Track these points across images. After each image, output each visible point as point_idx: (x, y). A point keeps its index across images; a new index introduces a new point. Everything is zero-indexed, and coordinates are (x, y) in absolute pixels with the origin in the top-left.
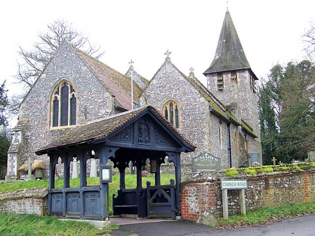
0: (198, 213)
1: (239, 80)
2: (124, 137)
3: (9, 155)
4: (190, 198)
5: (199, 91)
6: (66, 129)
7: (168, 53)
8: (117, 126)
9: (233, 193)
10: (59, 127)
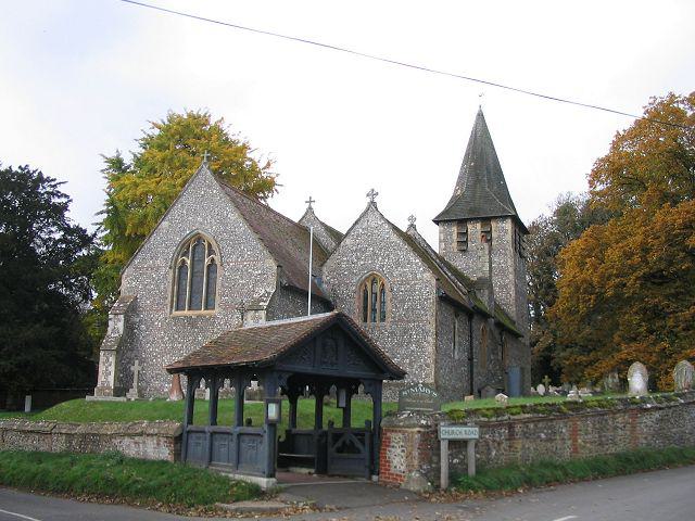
1: (494, 235)
3: (102, 353)
4: (393, 450)
7: (373, 194)
9: (458, 445)
10: (186, 312)
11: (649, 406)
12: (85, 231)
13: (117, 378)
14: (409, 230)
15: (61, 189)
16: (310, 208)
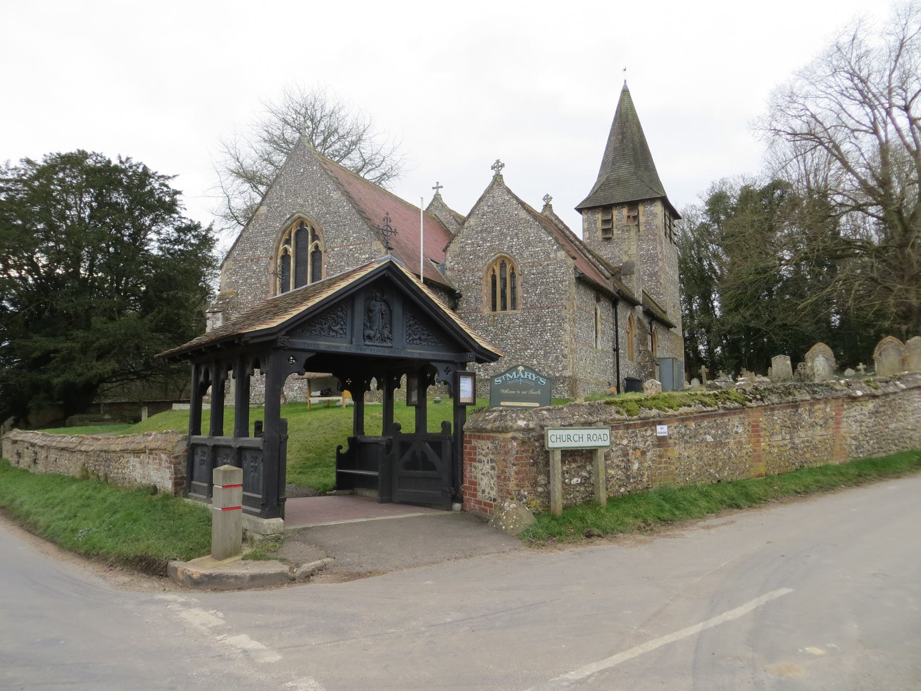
0: (495, 500)
1: (642, 219)
2: (330, 328)
4: (480, 466)
5: (556, 239)
7: (498, 166)
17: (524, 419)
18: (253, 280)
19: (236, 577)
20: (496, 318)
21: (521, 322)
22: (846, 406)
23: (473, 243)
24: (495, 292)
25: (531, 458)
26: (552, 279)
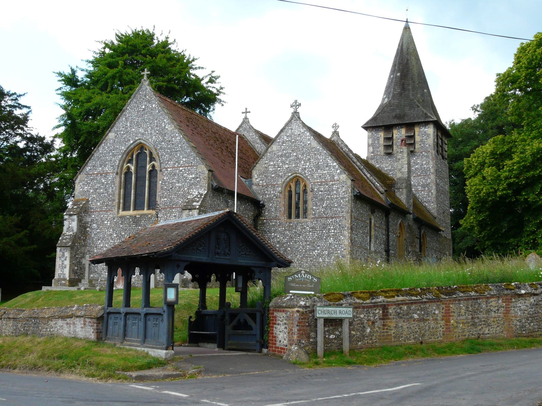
0: (286, 346)
1: (418, 138)
2: (197, 249)
3: (58, 249)
4: (278, 327)
6: (142, 215)
7: (296, 105)
8: (187, 237)
10: (131, 212)
11: (523, 292)
12: (44, 138)
13: (72, 271)
14: (332, 136)
15: (21, 101)
16: (246, 118)
17: (304, 301)
18: (102, 190)
19: (250, 317)
20: (291, 224)
21: (311, 228)
22: (513, 300)
23: (275, 165)
24: (291, 204)
25: (307, 322)
26: (335, 196)
